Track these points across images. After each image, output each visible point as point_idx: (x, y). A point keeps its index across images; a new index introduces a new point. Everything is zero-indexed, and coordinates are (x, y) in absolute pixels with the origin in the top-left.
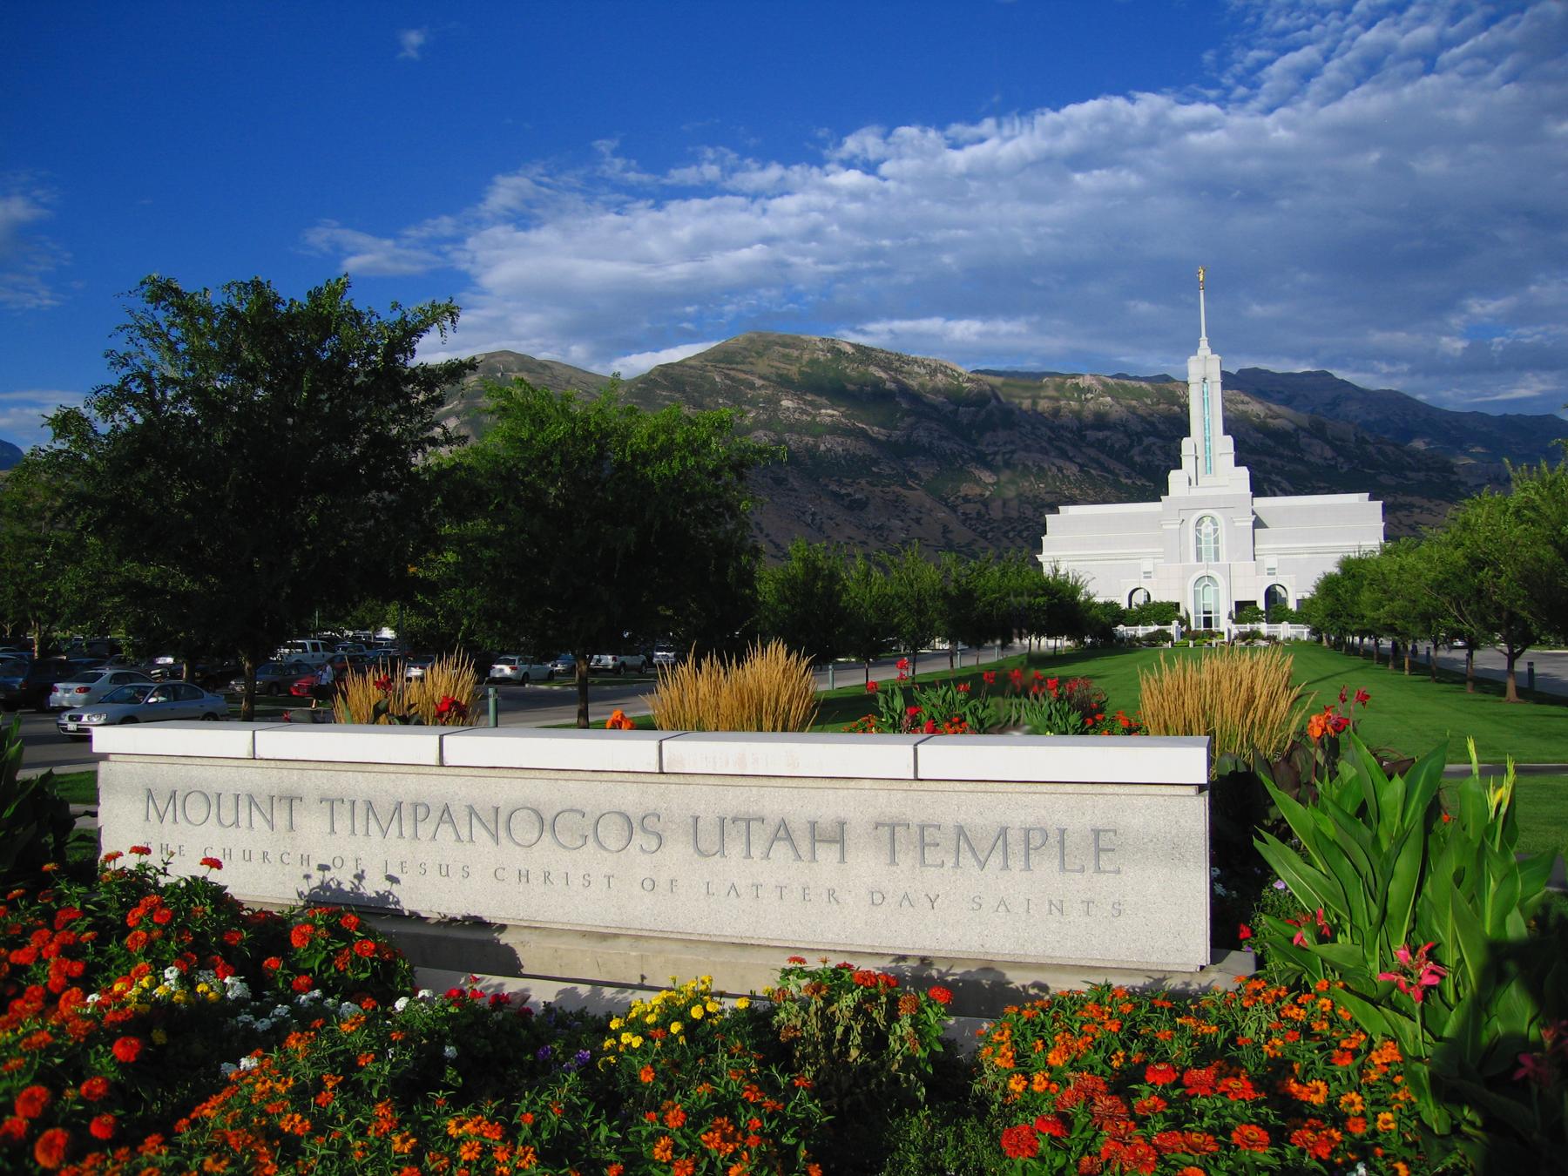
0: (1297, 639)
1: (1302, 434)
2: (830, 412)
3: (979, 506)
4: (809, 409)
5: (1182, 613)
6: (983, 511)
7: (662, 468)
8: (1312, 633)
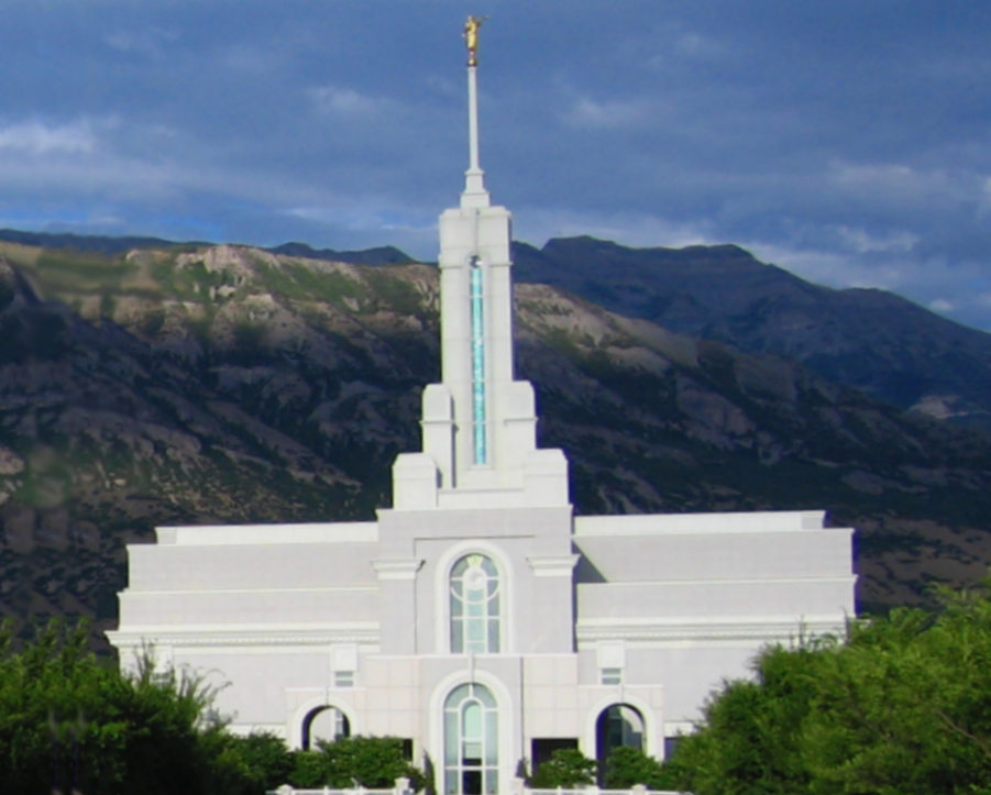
1: (682, 381)
5: (417, 762)
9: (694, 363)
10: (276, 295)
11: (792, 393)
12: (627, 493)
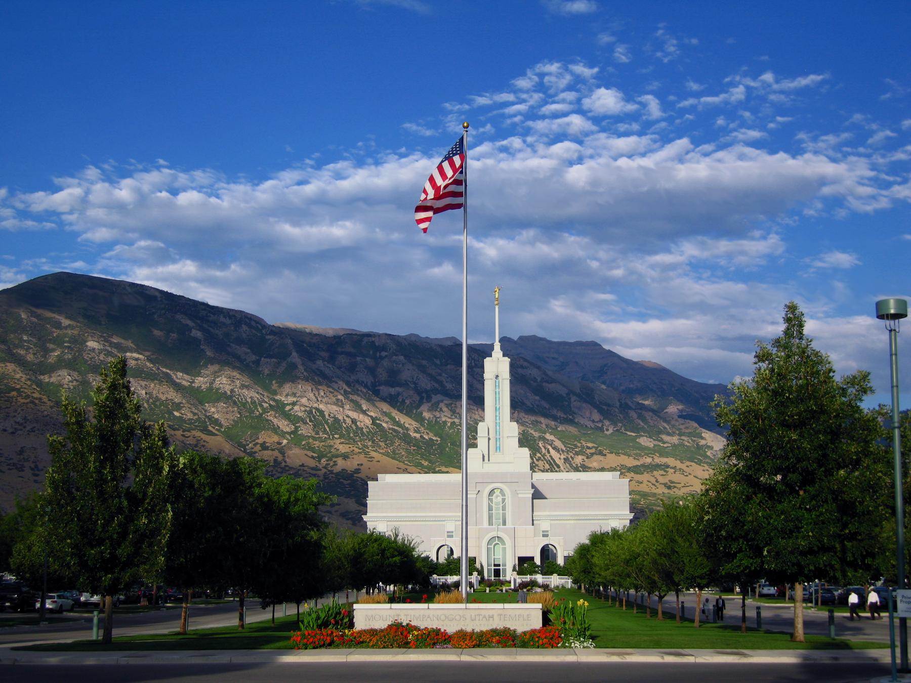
0: (563, 587)
1: (573, 398)
2: (135, 355)
3: (276, 453)
4: (115, 351)
5: (478, 565)
6: (280, 458)
7: (297, 509)
8: (575, 582)
9: (578, 391)
10: (405, 357)
11: (618, 404)
12: (551, 445)
